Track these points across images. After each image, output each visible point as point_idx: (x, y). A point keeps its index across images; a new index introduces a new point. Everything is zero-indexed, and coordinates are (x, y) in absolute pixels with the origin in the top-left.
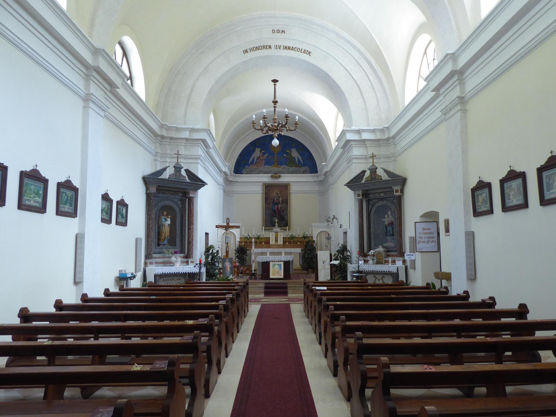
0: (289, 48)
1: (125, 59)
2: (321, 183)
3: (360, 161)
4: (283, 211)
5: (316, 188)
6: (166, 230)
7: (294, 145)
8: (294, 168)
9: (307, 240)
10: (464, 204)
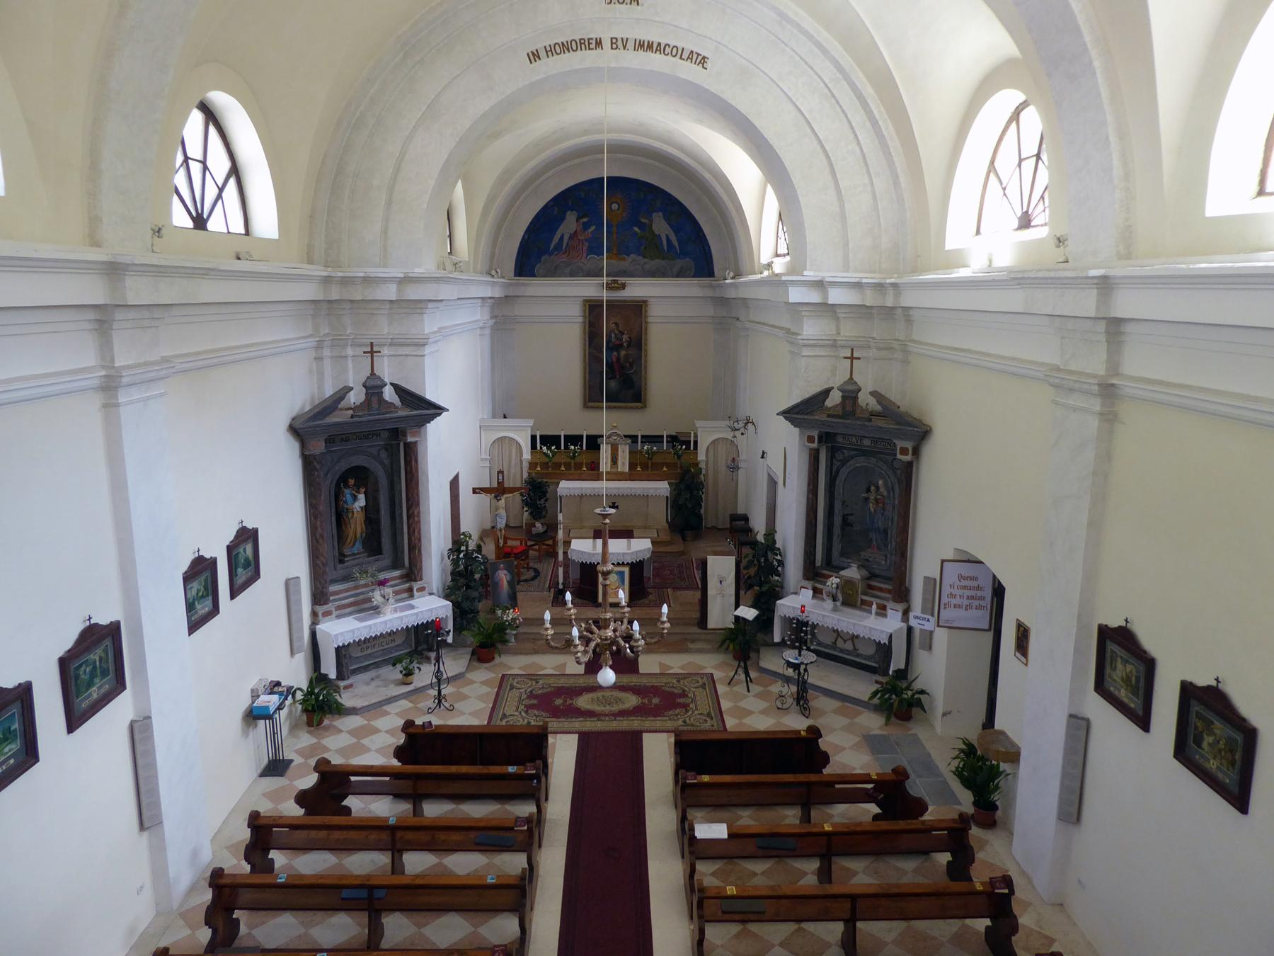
0: (650, 46)
1: (212, 129)
3: (818, 352)
4: (631, 365)
5: (710, 311)
6: (357, 525)
8: (657, 263)
10: (1076, 650)
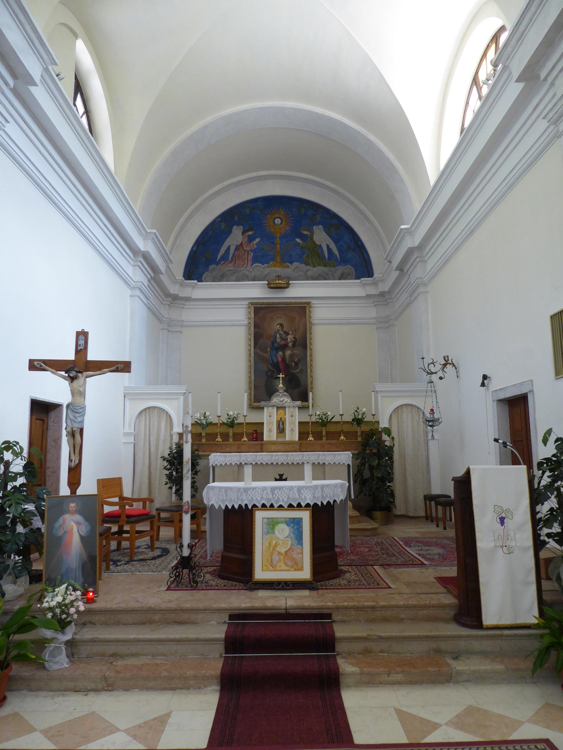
2: (383, 298)
4: (297, 364)
5: (372, 313)
7: (318, 217)
8: (319, 269)
9: (365, 428)
